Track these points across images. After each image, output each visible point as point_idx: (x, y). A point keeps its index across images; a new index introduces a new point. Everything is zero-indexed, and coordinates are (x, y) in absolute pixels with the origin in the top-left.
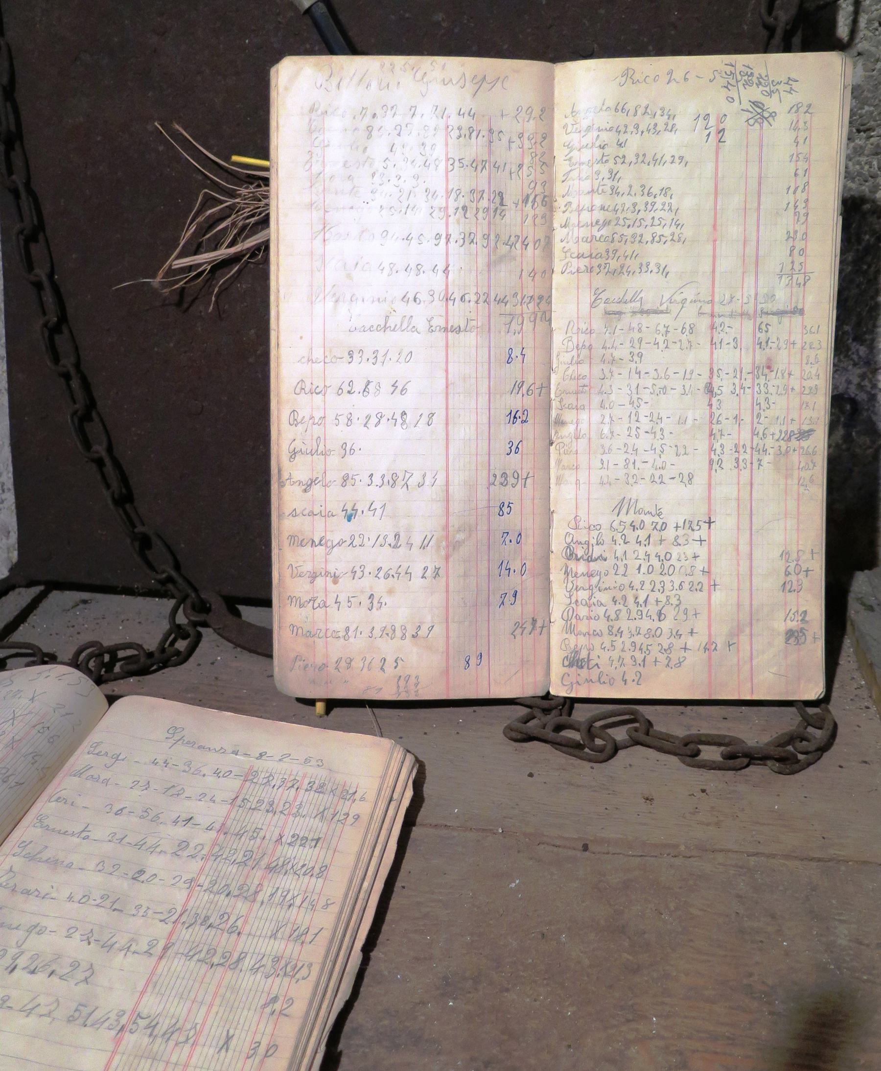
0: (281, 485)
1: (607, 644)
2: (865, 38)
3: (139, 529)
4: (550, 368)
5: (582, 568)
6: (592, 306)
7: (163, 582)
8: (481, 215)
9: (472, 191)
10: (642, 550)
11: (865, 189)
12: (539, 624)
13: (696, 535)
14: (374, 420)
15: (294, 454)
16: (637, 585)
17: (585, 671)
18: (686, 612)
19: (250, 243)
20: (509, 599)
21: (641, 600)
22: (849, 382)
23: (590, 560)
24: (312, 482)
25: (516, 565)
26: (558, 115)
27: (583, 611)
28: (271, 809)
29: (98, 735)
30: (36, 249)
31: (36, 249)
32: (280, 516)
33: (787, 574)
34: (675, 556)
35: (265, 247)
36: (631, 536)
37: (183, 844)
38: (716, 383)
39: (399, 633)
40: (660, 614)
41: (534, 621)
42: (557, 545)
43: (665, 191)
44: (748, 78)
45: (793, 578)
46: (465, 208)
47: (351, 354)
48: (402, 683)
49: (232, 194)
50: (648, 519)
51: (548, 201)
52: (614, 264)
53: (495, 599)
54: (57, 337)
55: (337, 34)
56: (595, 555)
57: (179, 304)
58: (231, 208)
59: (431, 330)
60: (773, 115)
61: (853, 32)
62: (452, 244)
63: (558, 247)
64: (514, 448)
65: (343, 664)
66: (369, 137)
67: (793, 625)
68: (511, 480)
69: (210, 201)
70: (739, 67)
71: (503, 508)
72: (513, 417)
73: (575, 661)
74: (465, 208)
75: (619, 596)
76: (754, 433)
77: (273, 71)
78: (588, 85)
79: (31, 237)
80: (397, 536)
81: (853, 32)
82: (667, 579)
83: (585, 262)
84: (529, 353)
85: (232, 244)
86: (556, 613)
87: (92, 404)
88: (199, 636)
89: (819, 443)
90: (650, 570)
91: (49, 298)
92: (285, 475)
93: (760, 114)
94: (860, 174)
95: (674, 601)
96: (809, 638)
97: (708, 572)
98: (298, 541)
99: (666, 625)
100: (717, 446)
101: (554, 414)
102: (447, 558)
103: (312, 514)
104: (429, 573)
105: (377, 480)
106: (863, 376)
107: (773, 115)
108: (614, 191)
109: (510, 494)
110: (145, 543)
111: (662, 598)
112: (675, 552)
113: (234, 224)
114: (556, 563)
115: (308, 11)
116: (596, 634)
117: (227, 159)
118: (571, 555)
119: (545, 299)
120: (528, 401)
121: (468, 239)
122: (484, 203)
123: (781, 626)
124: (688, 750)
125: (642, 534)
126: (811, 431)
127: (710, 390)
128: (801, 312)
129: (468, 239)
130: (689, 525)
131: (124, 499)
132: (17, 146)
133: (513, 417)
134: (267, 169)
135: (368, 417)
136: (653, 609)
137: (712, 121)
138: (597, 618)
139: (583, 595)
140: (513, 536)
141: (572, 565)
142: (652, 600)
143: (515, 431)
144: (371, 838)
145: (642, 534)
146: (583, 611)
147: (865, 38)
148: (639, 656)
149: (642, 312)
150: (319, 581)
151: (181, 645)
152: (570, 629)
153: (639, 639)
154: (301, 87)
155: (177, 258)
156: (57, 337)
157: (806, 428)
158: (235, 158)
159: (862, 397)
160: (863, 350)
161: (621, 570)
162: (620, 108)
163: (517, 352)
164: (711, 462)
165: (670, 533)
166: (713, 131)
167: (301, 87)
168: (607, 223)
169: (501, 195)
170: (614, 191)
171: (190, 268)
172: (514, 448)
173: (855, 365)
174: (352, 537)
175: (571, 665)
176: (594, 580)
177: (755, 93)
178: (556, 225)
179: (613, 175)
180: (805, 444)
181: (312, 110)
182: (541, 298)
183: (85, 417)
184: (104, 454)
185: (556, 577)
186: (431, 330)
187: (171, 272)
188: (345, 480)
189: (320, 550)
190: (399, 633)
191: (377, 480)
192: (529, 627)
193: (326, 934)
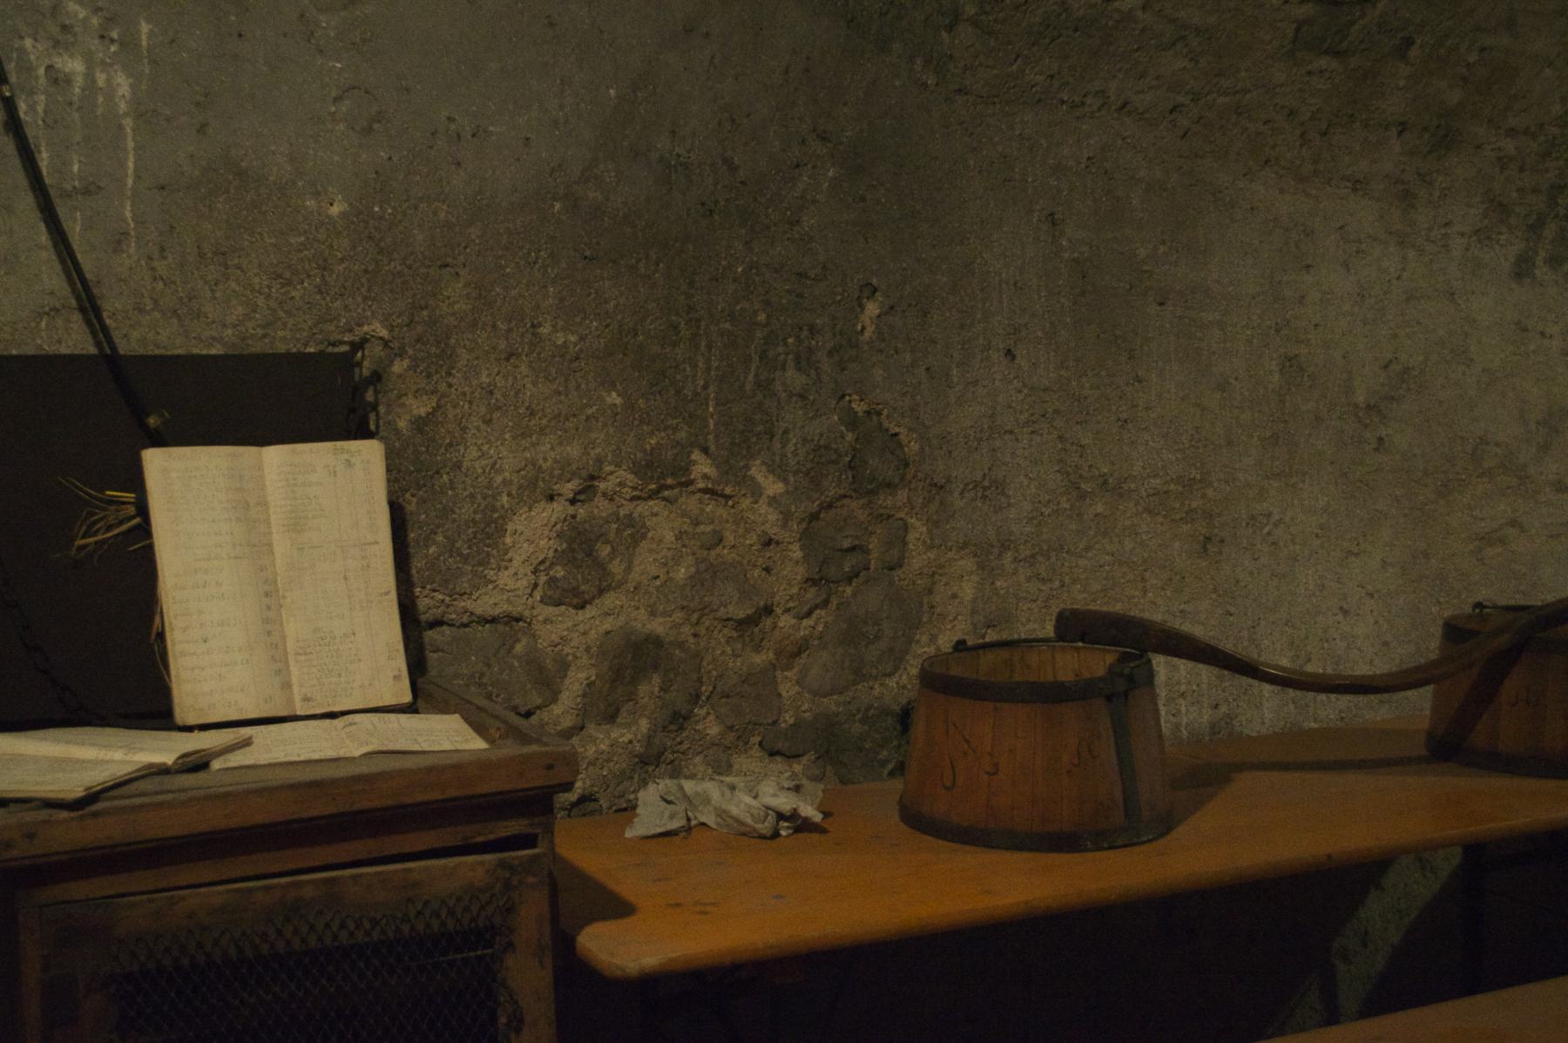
32: (174, 644)
44: (343, 451)
49: (104, 509)
61: (377, 427)
69: (94, 514)
71: (269, 633)
73: (306, 699)
78: (275, 457)
81: (377, 427)
86: (294, 680)
89: (393, 596)
93: (349, 464)
98: (183, 654)
104: (1396, 367)
129: (238, 519)
130: (345, 635)
172: (269, 608)
185: (292, 663)
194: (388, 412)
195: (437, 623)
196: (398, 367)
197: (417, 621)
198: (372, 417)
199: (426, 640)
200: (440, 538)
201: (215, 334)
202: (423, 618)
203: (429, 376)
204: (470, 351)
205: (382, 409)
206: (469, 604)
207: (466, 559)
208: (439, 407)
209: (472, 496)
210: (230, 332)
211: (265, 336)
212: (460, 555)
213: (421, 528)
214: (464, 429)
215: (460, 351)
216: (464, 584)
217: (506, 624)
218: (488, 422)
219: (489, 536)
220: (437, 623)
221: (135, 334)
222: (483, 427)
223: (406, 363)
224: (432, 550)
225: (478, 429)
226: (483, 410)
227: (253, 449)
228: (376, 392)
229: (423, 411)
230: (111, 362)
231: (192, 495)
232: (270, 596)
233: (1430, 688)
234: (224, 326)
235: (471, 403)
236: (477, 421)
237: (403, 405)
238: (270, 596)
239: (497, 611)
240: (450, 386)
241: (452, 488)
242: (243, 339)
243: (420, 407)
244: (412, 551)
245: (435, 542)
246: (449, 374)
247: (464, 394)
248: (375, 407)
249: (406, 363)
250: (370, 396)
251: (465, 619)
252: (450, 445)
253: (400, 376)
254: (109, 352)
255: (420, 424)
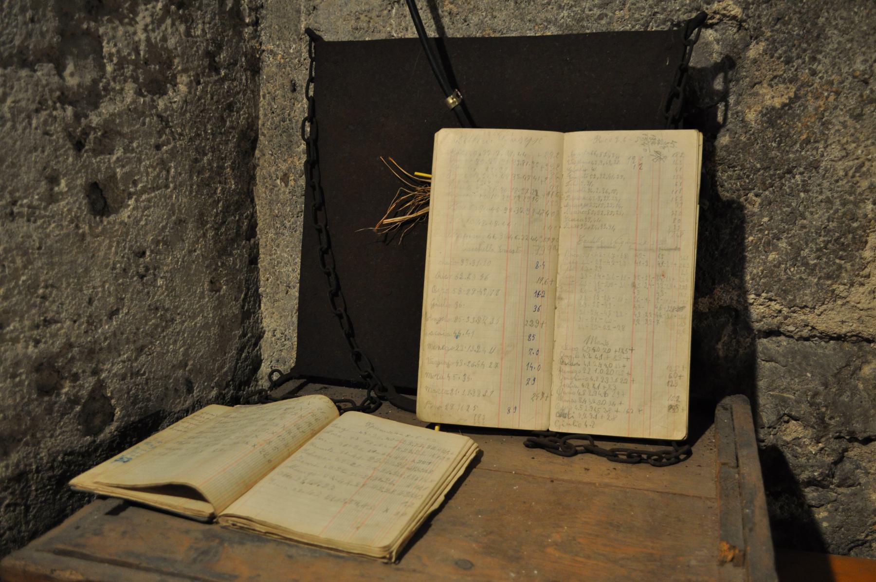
0: (426, 320)
1: (578, 407)
2: (731, 122)
3: (356, 349)
4: (557, 272)
5: (567, 368)
6: (578, 244)
7: (364, 377)
8: (526, 200)
9: (523, 189)
10: (597, 362)
11: (734, 196)
12: (545, 395)
13: (625, 356)
14: (471, 292)
15: (433, 306)
16: (594, 378)
17: (566, 420)
18: (618, 393)
19: (420, 213)
20: (531, 381)
21: (596, 386)
22: (732, 299)
23: (571, 365)
24: (441, 319)
25: (535, 365)
26: (565, 156)
27: (567, 390)
28: (411, 452)
29: (334, 422)
30: (320, 214)
31: (320, 214)
32: (425, 334)
33: (670, 377)
34: (614, 365)
35: (426, 215)
36: (593, 354)
37: (372, 458)
38: (637, 282)
39: (476, 394)
40: (605, 394)
41: (543, 394)
42: (557, 357)
43: (614, 191)
44: (654, 140)
45: (673, 379)
46: (519, 197)
47: (462, 261)
48: (477, 418)
49: (414, 190)
50: (601, 347)
51: (559, 195)
52: (589, 224)
53: (525, 381)
54: (325, 256)
55: (466, 118)
56: (575, 362)
57: (384, 242)
58: (412, 197)
59: (500, 251)
60: (666, 157)
62: (512, 213)
63: (563, 215)
64: (537, 309)
65: (449, 407)
66: (477, 164)
67: (673, 403)
68: (535, 324)
69: (403, 193)
70: (649, 136)
71: (531, 337)
72: (538, 294)
73: (562, 415)
74: (519, 197)
75: (585, 383)
76: (655, 307)
77: (436, 135)
78: (581, 141)
79: (318, 208)
80: (479, 347)
82: (609, 376)
83: (576, 223)
84: (546, 264)
85: (411, 213)
86: (554, 392)
87: (339, 287)
88: (381, 404)
90: (602, 371)
91: (324, 237)
92: (429, 315)
94: (731, 189)
95: (613, 387)
96: (680, 410)
97: (630, 374)
99: (608, 399)
100: (637, 313)
101: (558, 294)
102: (502, 359)
103: (440, 334)
105: (471, 320)
106: (739, 296)
107: (666, 157)
108: (590, 191)
109: (533, 331)
110: (358, 357)
111: (607, 386)
112: (614, 363)
113: (413, 204)
114: (556, 366)
115: (453, 109)
116: (573, 401)
117: (413, 174)
118: (563, 363)
119: (555, 240)
120: (545, 287)
121: (520, 210)
122: (528, 195)
123: (667, 403)
124: (612, 456)
125: (598, 354)
126: (683, 307)
127: (634, 285)
128: (679, 249)
131: (350, 335)
132: (316, 167)
133: (538, 294)
134: (430, 179)
135: (469, 290)
136: (602, 391)
137: (637, 160)
138: (574, 393)
139: (567, 382)
140: (535, 351)
141: (563, 367)
142: (601, 386)
143: (538, 301)
144: (454, 465)
145: (598, 354)
146: (567, 390)
147: (731, 122)
148: (594, 414)
149: (602, 247)
150: (441, 366)
151: (372, 406)
152: (560, 398)
153: (594, 405)
154: (448, 142)
155: (387, 218)
156: (325, 256)
157: (681, 305)
158: (416, 173)
159: (740, 308)
160: (737, 281)
161: (587, 371)
162: (594, 153)
163: (541, 263)
164: (634, 320)
165: (612, 354)
166: (637, 164)
167: (448, 142)
168: (586, 205)
169: (536, 191)
170: (590, 191)
171: (391, 224)
173: (733, 289)
174: (458, 346)
175: (560, 416)
176: (574, 375)
177: (657, 147)
178: (562, 205)
179: (589, 183)
180: (680, 313)
181: (452, 152)
182: (554, 239)
183: (334, 295)
184: (343, 311)
185: (555, 372)
186: (500, 251)
187: (382, 225)
188: (456, 318)
189: (442, 351)
190: (476, 394)
191: (471, 320)
192: (540, 396)
193: (430, 490)
194: (737, 103)
195: (770, 333)
196: (754, 51)
197: (749, 329)
198: (721, 107)
199: (760, 348)
200: (783, 244)
201: (550, 16)
202: (757, 326)
203: (788, 62)
204: (844, 32)
205: (732, 100)
206: (812, 319)
207: (812, 270)
208: (797, 97)
209: (829, 201)
210: (565, 13)
211: (600, 17)
212: (806, 264)
213: (760, 231)
214: (825, 124)
215: (830, 32)
216: (806, 296)
217: (854, 343)
218: (858, 117)
219: (843, 247)
220: (770, 333)
221: (474, 19)
222: (850, 122)
223: (762, 46)
224: (772, 256)
225: (844, 125)
226: (852, 102)
227: (561, 133)
228: (727, 81)
229: (777, 103)
230: (441, 41)
231: (474, 174)
232: (545, 294)
233: (416, 36)
234: (560, 7)
235: (838, 93)
236: (842, 116)
237: (757, 94)
238: (545, 294)
239: (844, 330)
240: (814, 73)
241: (806, 191)
242: (581, 20)
243: (774, 97)
244: (749, 255)
245: (776, 248)
246: (814, 59)
247: (831, 83)
248: (724, 96)
249: (762, 46)
250: (718, 85)
251: (805, 332)
252: (807, 141)
253: (755, 61)
254: (432, 33)
255: (771, 116)
